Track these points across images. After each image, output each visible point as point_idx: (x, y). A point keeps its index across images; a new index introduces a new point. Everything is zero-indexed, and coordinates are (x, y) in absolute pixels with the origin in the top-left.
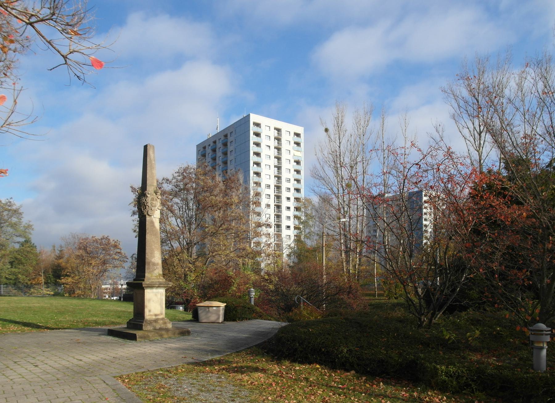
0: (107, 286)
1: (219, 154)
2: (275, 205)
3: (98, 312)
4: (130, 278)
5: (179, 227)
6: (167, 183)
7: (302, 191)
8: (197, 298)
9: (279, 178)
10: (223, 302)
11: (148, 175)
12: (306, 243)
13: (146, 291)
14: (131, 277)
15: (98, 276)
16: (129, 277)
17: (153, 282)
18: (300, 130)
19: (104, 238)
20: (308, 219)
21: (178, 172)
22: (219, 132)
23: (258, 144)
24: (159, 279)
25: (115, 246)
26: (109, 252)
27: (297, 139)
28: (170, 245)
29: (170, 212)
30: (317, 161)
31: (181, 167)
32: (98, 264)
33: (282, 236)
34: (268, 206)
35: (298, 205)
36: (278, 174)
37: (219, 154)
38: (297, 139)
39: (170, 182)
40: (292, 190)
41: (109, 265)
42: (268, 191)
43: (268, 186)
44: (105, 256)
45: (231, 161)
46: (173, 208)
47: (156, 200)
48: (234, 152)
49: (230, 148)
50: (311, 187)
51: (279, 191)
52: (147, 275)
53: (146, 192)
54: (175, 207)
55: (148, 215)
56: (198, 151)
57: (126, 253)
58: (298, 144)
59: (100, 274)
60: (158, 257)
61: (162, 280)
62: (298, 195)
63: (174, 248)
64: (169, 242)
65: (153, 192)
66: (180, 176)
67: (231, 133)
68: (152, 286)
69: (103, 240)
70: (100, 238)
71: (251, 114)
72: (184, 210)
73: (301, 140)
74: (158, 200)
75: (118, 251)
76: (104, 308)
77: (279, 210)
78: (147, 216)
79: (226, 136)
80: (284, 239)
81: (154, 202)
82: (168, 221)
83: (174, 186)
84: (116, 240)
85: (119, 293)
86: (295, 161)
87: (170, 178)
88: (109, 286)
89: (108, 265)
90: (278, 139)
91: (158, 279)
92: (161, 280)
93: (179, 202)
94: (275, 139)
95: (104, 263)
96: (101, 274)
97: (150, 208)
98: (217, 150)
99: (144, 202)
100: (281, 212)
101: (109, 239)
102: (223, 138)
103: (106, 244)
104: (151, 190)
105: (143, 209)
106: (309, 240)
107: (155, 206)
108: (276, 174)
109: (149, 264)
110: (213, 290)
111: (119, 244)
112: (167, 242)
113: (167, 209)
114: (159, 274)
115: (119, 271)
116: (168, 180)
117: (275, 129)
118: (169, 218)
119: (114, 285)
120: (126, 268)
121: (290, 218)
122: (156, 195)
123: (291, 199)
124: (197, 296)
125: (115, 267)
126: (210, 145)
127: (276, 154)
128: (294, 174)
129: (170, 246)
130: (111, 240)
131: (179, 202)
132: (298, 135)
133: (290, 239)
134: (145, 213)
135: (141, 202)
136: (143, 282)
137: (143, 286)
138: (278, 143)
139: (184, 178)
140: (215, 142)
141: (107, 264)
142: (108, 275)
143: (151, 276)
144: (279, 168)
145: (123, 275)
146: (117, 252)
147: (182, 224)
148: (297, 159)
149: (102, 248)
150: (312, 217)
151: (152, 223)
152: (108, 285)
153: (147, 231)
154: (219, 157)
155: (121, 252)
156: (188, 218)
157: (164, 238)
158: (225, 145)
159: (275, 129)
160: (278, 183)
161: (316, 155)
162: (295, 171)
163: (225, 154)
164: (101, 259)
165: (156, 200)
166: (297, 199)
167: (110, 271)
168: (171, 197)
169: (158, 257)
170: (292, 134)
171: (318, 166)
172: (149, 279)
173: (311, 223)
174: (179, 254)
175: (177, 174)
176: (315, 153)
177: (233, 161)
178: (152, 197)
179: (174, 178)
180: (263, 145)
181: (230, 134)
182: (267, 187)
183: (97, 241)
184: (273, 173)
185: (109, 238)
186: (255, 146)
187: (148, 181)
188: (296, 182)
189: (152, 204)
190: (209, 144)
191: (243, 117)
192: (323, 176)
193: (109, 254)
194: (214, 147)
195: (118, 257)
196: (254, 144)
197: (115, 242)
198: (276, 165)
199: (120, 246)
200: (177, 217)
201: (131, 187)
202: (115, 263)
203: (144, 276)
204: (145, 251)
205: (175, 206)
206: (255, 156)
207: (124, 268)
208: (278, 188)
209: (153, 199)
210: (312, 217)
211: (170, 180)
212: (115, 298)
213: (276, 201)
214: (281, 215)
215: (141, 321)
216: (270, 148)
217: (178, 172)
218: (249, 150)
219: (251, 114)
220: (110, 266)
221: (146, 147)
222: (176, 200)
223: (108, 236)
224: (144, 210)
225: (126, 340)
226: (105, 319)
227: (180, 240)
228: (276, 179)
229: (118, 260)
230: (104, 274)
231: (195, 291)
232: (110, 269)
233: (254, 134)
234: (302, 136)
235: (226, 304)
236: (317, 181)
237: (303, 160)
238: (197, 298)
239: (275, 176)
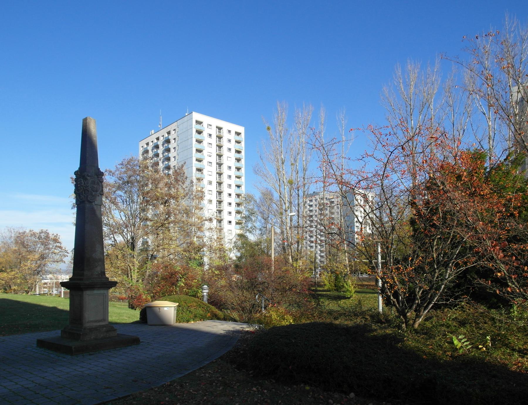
6: (110, 175)
10: (174, 301)
18: (241, 129)
19: (42, 232)
21: (121, 164)
25: (56, 240)
27: (238, 138)
28: (113, 239)
29: (113, 205)
31: (124, 159)
34: (210, 201)
35: (238, 201)
39: (113, 174)
42: (209, 187)
46: (116, 200)
54: (119, 200)
62: (238, 191)
63: (118, 241)
64: (112, 236)
75: (58, 244)
80: (226, 234)
81: (96, 186)
82: (111, 214)
83: (118, 178)
87: (113, 170)
88: (49, 281)
93: (122, 194)
101: (48, 233)
107: (97, 191)
111: (59, 238)
112: (110, 236)
113: (110, 201)
116: (111, 172)
117: (217, 127)
118: (112, 211)
129: (113, 241)
131: (122, 194)
132: (238, 134)
139: (128, 169)
146: (56, 246)
147: (126, 217)
149: (41, 242)
156: (132, 212)
157: (106, 231)
166: (238, 196)
168: (114, 189)
179: (117, 169)
182: (209, 183)
183: (35, 235)
185: (48, 232)
195: (58, 251)
200: (121, 211)
205: (119, 199)
207: (65, 262)
211: (113, 171)
217: (121, 164)
222: (119, 192)
223: (47, 230)
227: (124, 234)
235: (178, 304)
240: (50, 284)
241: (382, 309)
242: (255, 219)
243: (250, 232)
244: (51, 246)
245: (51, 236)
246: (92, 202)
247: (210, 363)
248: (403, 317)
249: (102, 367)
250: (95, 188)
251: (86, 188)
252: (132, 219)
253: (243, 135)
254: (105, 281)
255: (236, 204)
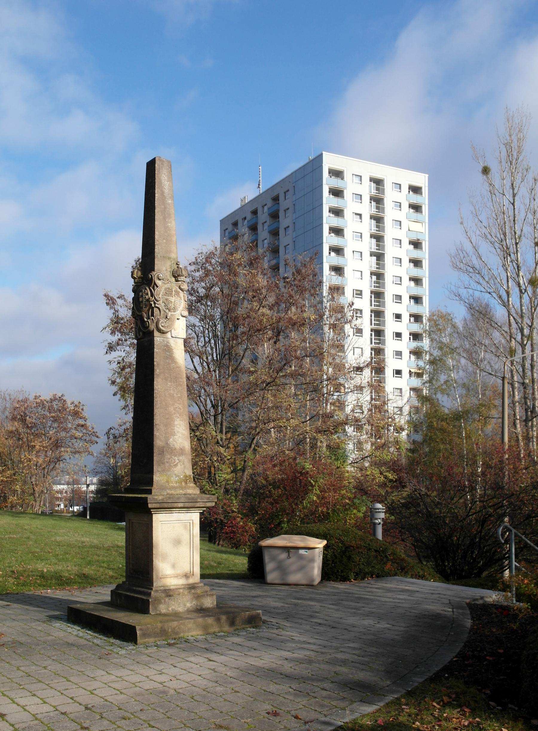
0: (62, 487)
1: (263, 234)
2: (372, 330)
3: (48, 549)
4: (102, 472)
5: (197, 373)
7: (426, 300)
8: (238, 517)
9: (379, 276)
10: (317, 536)
11: (157, 233)
12: (440, 402)
13: (154, 515)
14: (104, 471)
15: (46, 470)
16: (100, 470)
17: (171, 496)
20: (445, 354)
21: (194, 263)
22: (262, 193)
23: (337, 212)
24: (185, 488)
25: (76, 414)
26: (64, 425)
27: (415, 199)
30: (465, 235)
31: (200, 252)
32: (46, 447)
33: (386, 389)
35: (416, 328)
36: (377, 268)
37: (263, 234)
38: (415, 199)
40: (406, 299)
41: (65, 449)
43: (359, 293)
44: (57, 432)
45: (285, 247)
47: (177, 293)
48: (291, 229)
49: (284, 222)
50: (453, 288)
51: (379, 302)
52: (157, 478)
53: (153, 273)
55: (159, 330)
56: (224, 231)
57: (95, 426)
58: (416, 208)
59: (49, 465)
60: (183, 434)
61: (193, 490)
62: (416, 309)
65: (168, 275)
66: (198, 271)
67: (285, 193)
68: (170, 505)
69: (54, 403)
70: (48, 399)
71: (324, 152)
72: (207, 339)
73: (424, 200)
74: (181, 294)
75: (82, 422)
76: (58, 539)
77: (380, 340)
78: (156, 333)
79: (276, 199)
84: (76, 403)
85: (83, 499)
86: (411, 243)
88: (65, 487)
89: (63, 449)
90: (378, 201)
91: (182, 488)
92: (190, 491)
94: (371, 199)
95: (57, 445)
96: (52, 466)
97: (162, 312)
98: (260, 227)
99: (148, 300)
100: (383, 342)
101: (65, 401)
102: (270, 203)
103: (60, 411)
104: (164, 269)
105: (145, 315)
106: (446, 396)
107: (175, 309)
108: (374, 269)
109: (162, 452)
110: (271, 500)
111: (82, 409)
114: (186, 476)
115: (84, 460)
117: (372, 180)
119: (73, 485)
120: (95, 455)
121: (401, 355)
122: (177, 281)
123: (403, 317)
124: (239, 513)
125: (75, 453)
126: (245, 218)
127: (374, 230)
128: (409, 267)
130: (69, 403)
132: (416, 190)
133: (401, 396)
134: (152, 327)
135: (141, 299)
136: (149, 496)
137: (150, 506)
138: (378, 208)
140: (255, 212)
141: (62, 446)
142: (63, 468)
143: (167, 482)
144: (379, 257)
145: (90, 466)
146: (78, 425)
148: (414, 238)
149: (52, 417)
150: (453, 350)
151: (168, 349)
152: (64, 484)
153: (157, 371)
154: (263, 241)
155: (85, 424)
158: (275, 216)
159: (372, 180)
160: (377, 287)
161: (462, 223)
162: (411, 261)
163: (275, 233)
164: (50, 439)
165: (177, 293)
167: (68, 461)
169: (183, 434)
170: (405, 188)
171: (468, 248)
172: (163, 488)
173: (450, 362)
174: (198, 428)
175: (193, 268)
176: (460, 220)
177: (290, 247)
178: (166, 286)
180: (348, 213)
181: (283, 194)
182: (357, 294)
184: (368, 267)
185: (64, 398)
186: (333, 216)
187: (156, 247)
188: (412, 283)
189: (167, 303)
190: (244, 217)
191: (307, 161)
192: (477, 266)
193: (65, 429)
194: (253, 221)
195: (81, 435)
196: (330, 211)
197: (76, 406)
198: (373, 250)
199: (85, 414)
201: (105, 295)
202: (76, 444)
203: (150, 482)
204: (153, 420)
206: (332, 234)
207: (92, 455)
208: (378, 295)
209: (169, 292)
210: (453, 350)
212: (76, 508)
213: (373, 322)
214: (384, 350)
215: (146, 590)
216: (361, 218)
217: (194, 263)
218: (322, 224)
219: (324, 153)
220: (67, 452)
221: (151, 166)
223: (62, 396)
224: (148, 318)
225: (112, 640)
226: (60, 568)
228: (374, 278)
229: (81, 439)
230: (57, 466)
231: (234, 502)
232: (66, 456)
233: (329, 192)
234: (425, 191)
235: (325, 542)
236: (465, 278)
237: (427, 239)
238: (238, 517)
239: (372, 274)
240: (66, 492)
241: (188, 492)
242: (455, 363)
243: (443, 392)
244: (70, 425)
245: (69, 405)
246: (167, 332)
247: (426, 680)
248: (476, 538)
249: (200, 676)
250: (171, 302)
251: (155, 303)
252: (215, 371)
253: (425, 191)
254: (193, 496)
255: (410, 334)
